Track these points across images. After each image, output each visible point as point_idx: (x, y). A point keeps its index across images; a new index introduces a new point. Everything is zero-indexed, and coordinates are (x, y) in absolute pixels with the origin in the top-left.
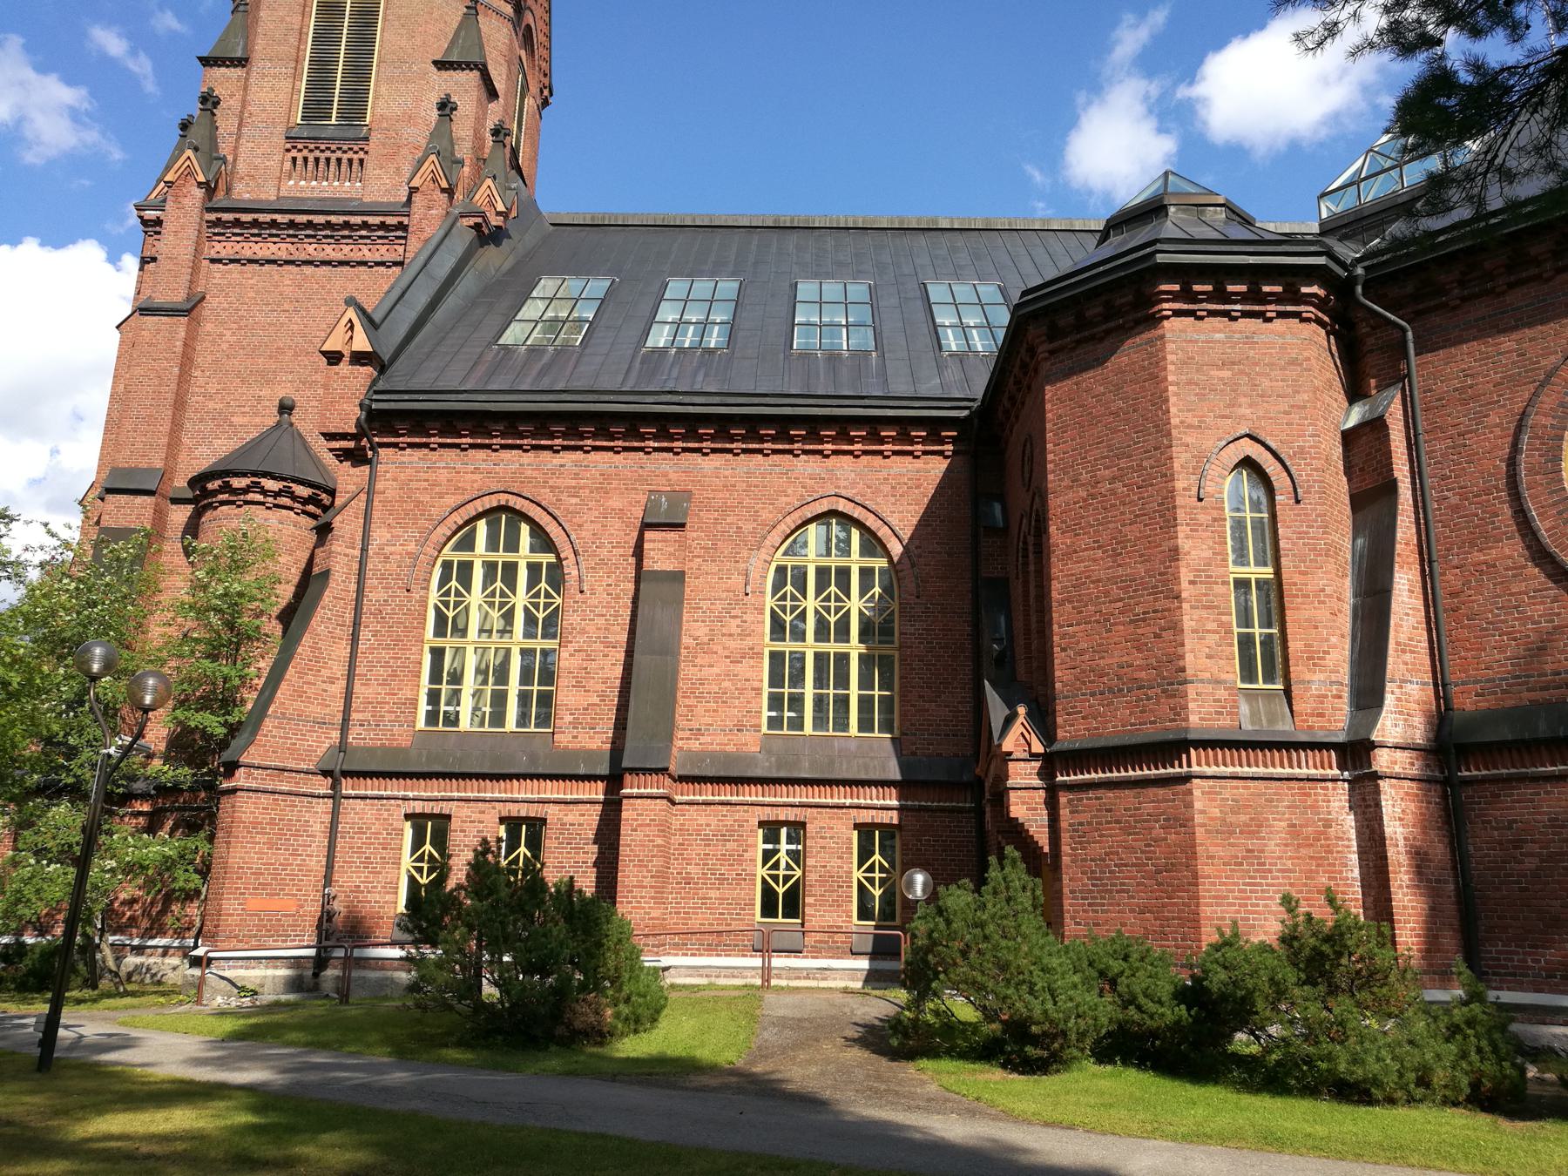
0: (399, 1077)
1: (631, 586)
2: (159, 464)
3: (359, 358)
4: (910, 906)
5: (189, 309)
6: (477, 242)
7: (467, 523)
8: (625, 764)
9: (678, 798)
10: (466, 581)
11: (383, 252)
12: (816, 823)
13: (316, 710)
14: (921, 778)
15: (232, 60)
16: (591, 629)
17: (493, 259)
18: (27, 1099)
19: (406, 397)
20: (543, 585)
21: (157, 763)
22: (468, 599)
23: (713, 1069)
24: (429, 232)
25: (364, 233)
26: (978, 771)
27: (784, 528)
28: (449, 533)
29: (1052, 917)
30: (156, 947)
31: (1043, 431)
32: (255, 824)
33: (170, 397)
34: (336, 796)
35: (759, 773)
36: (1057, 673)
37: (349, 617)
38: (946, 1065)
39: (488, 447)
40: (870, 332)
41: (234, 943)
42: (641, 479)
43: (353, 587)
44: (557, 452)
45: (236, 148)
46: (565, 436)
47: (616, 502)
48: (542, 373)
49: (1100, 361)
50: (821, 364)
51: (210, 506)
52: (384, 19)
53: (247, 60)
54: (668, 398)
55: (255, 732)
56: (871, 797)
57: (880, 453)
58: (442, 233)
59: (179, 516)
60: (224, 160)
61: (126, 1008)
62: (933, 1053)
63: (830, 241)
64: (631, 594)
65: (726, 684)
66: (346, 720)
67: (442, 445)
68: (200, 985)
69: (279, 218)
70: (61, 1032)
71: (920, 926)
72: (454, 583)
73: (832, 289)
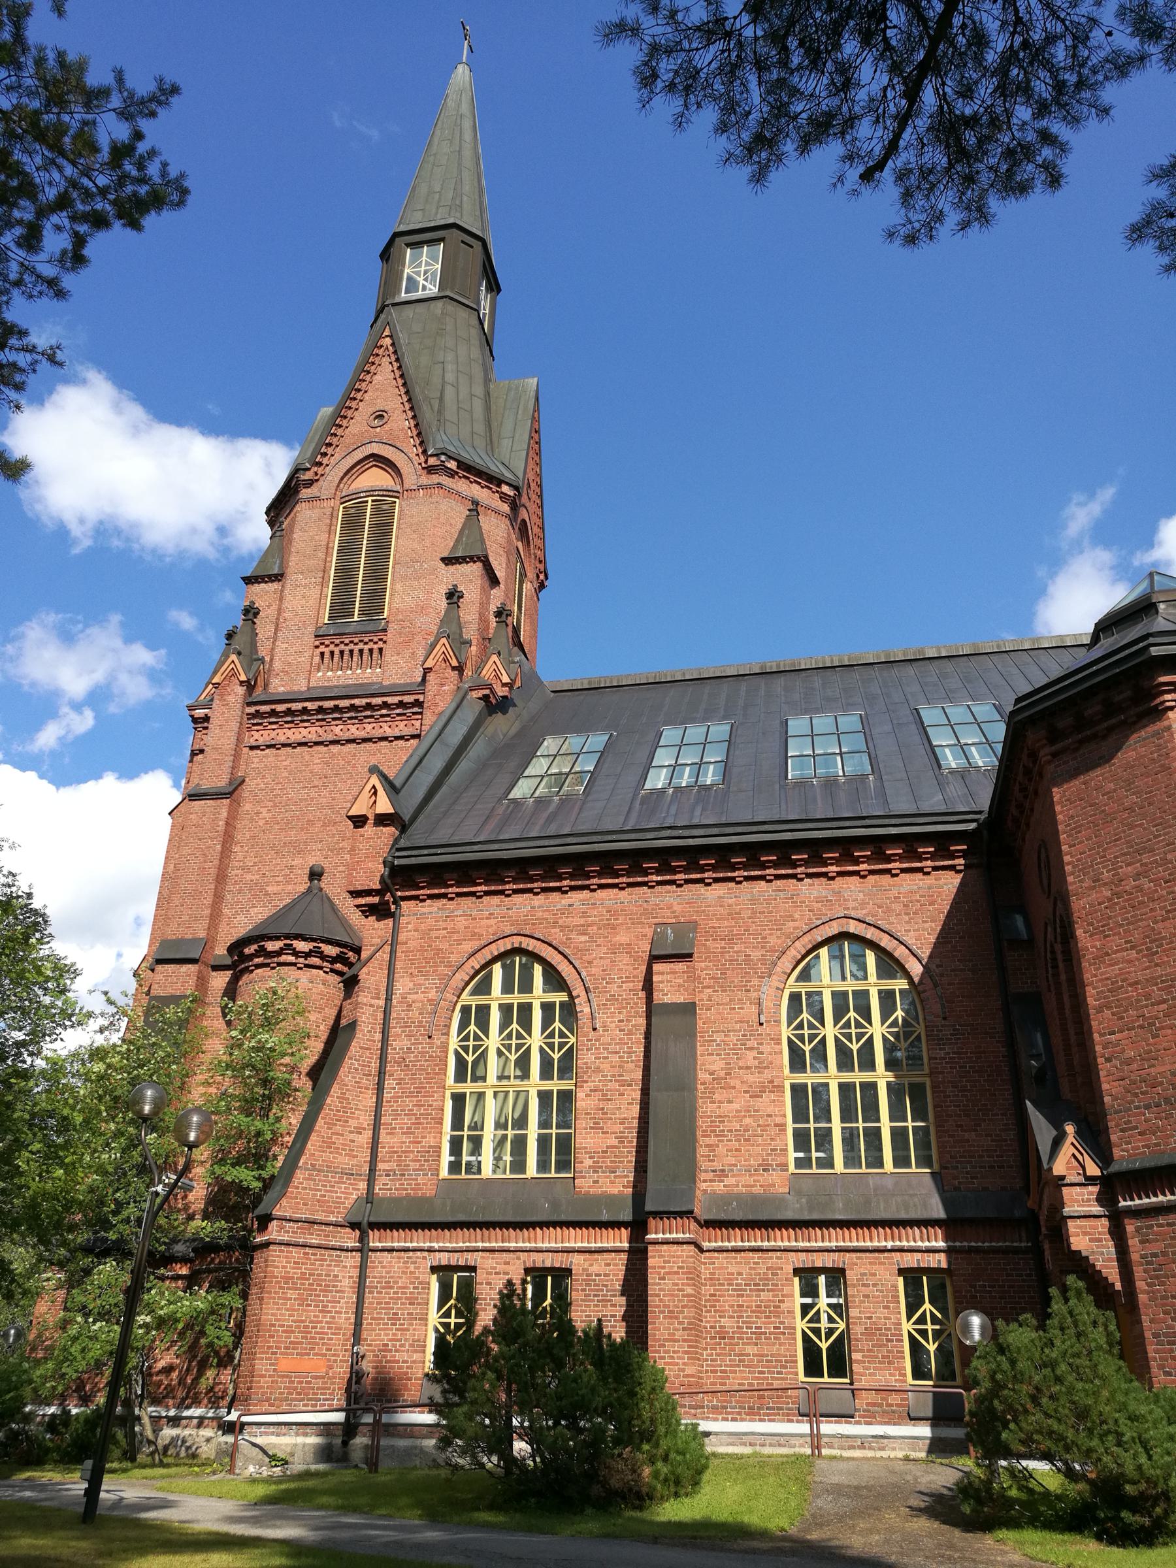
0: (432, 1535)
1: (642, 1021)
2: (202, 934)
3: (382, 820)
4: (968, 1352)
5: (231, 792)
6: (485, 711)
7: (483, 967)
8: (649, 1207)
9: (706, 1245)
10: (484, 1025)
11: (402, 727)
12: (856, 1269)
13: (343, 1161)
14: (968, 1215)
15: (269, 576)
16: (605, 1067)
17: (500, 725)
18: (74, 1543)
19: (426, 852)
20: (557, 1024)
21: (198, 1223)
22: (486, 1042)
23: (763, 1534)
24: (442, 706)
25: (384, 712)
26: (1030, 1204)
27: (794, 953)
28: (467, 978)
29: (1132, 1352)
30: (191, 1418)
31: (1056, 833)
32: (287, 1279)
33: (213, 871)
34: (363, 1250)
35: (789, 1215)
36: (1105, 1086)
37: (374, 1066)
38: (1030, 1535)
39: (502, 892)
40: (865, 757)
41: (266, 1407)
42: (646, 913)
43: (378, 1036)
44: (566, 892)
45: (273, 649)
46: (572, 877)
47: (622, 938)
48: (550, 820)
49: (1107, 759)
50: (818, 790)
51: (247, 970)
52: (398, 528)
53: (282, 575)
54: (668, 833)
55: (287, 1184)
56: (914, 1238)
57: (888, 871)
58: (454, 705)
59: (220, 980)
60: (262, 660)
61: (163, 1477)
62: (1013, 1524)
63: (817, 680)
64: (643, 1029)
65: (747, 1121)
66: (372, 1170)
67: (459, 895)
68: (232, 1452)
69: (309, 705)
70: (103, 1495)
71: (980, 1368)
72: (472, 1027)
73: (822, 722)
